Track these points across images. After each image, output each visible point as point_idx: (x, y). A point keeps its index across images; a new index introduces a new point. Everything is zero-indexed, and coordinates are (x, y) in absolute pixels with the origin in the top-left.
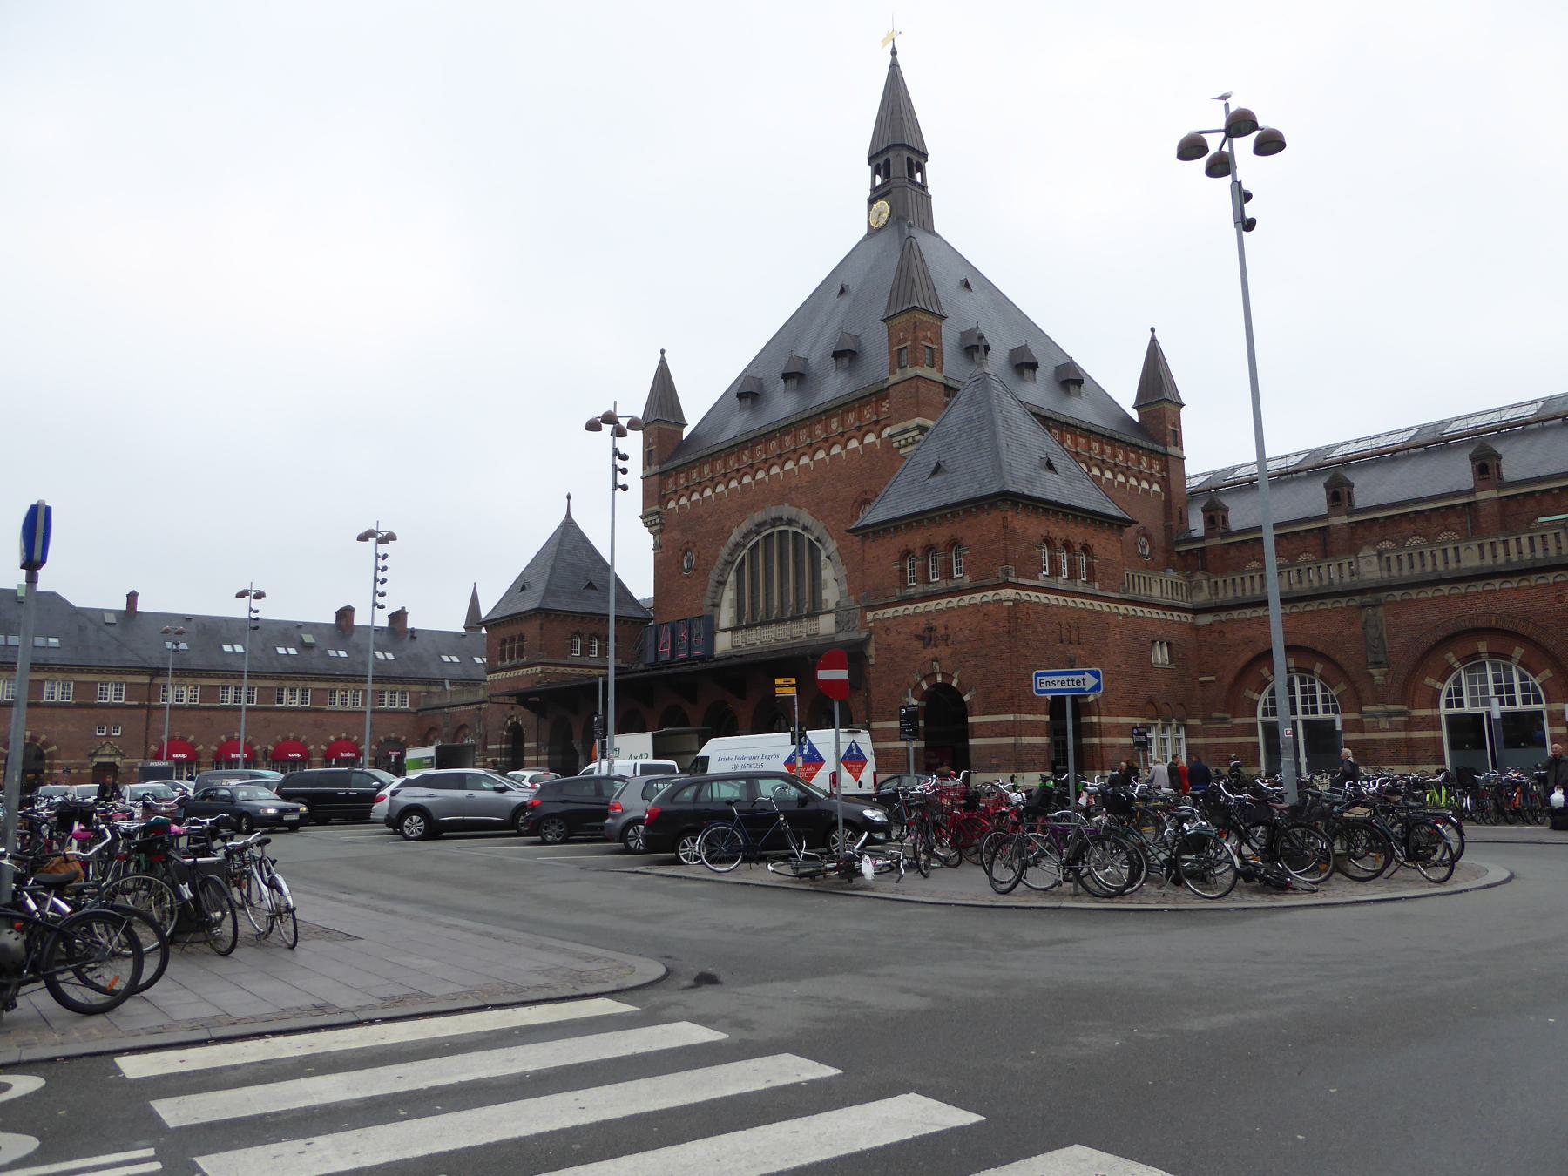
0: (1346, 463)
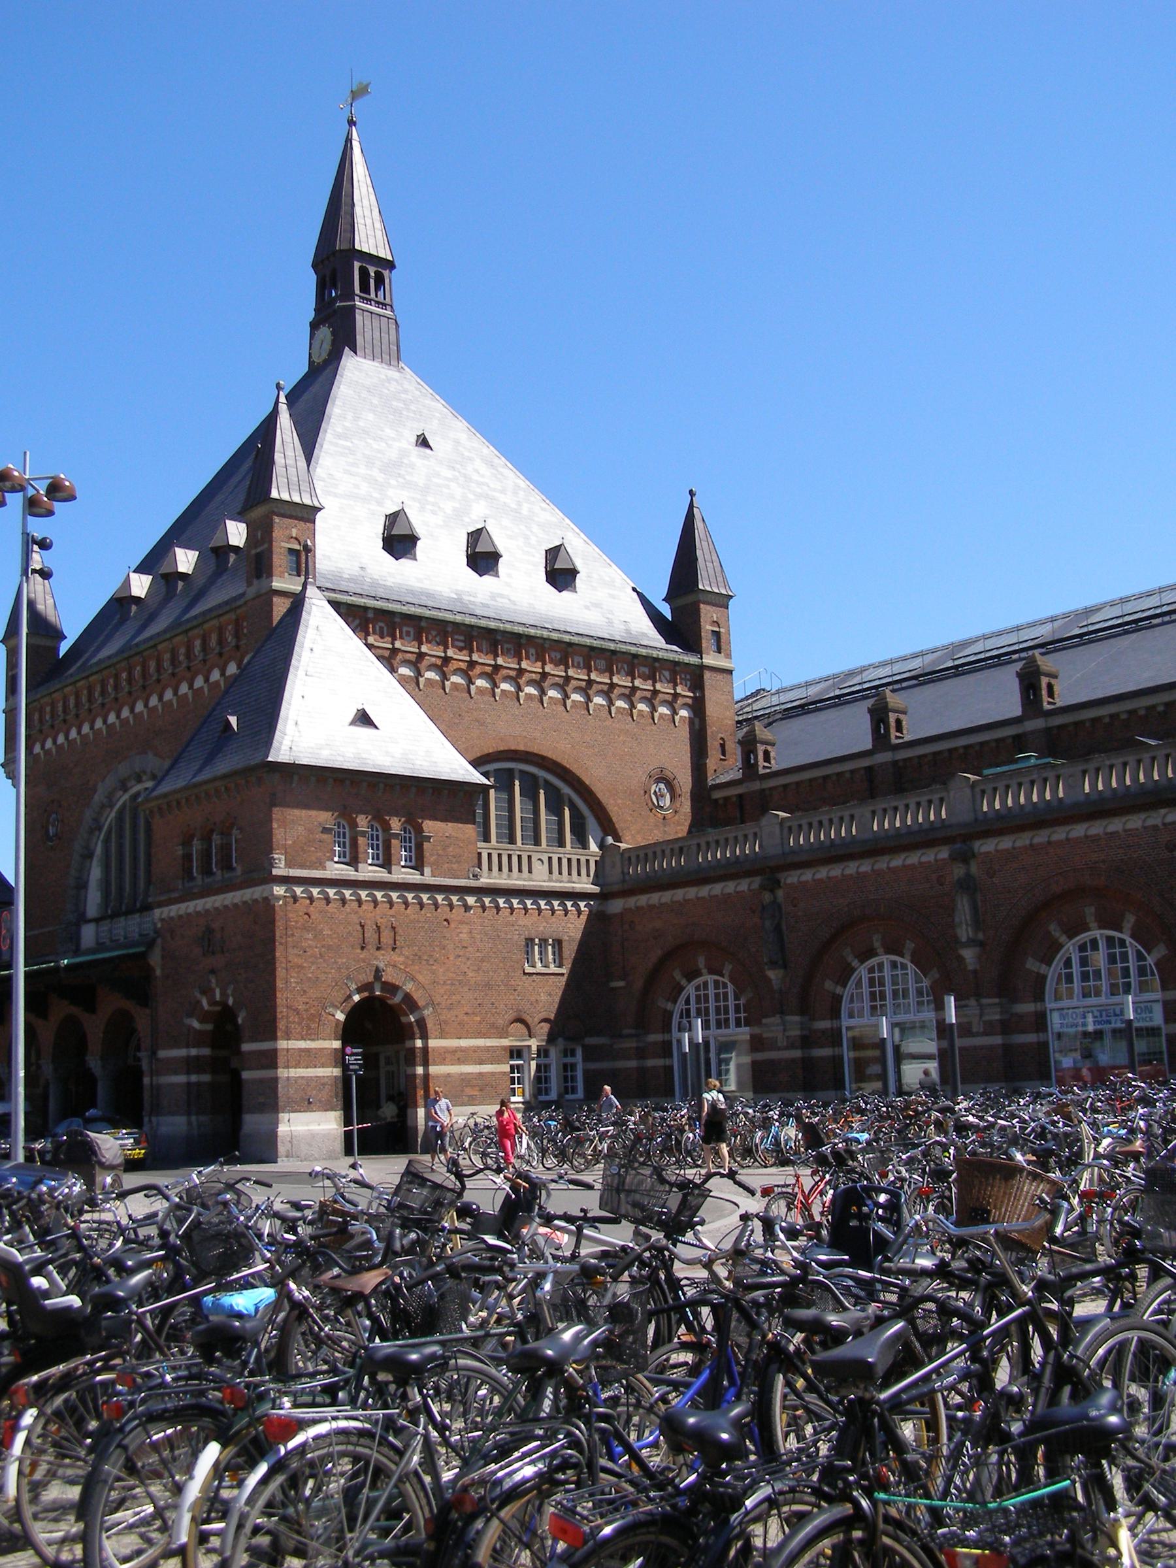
0: (877, 689)
